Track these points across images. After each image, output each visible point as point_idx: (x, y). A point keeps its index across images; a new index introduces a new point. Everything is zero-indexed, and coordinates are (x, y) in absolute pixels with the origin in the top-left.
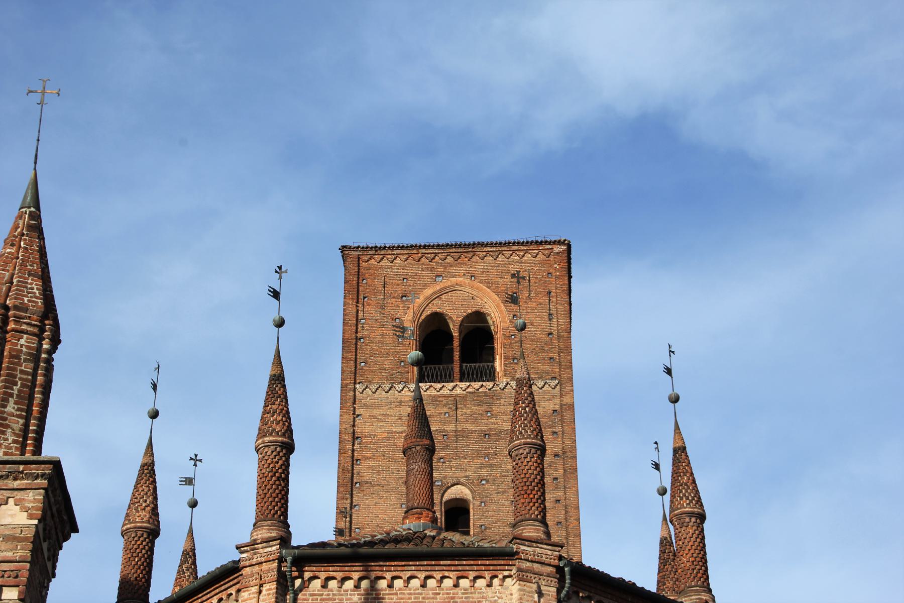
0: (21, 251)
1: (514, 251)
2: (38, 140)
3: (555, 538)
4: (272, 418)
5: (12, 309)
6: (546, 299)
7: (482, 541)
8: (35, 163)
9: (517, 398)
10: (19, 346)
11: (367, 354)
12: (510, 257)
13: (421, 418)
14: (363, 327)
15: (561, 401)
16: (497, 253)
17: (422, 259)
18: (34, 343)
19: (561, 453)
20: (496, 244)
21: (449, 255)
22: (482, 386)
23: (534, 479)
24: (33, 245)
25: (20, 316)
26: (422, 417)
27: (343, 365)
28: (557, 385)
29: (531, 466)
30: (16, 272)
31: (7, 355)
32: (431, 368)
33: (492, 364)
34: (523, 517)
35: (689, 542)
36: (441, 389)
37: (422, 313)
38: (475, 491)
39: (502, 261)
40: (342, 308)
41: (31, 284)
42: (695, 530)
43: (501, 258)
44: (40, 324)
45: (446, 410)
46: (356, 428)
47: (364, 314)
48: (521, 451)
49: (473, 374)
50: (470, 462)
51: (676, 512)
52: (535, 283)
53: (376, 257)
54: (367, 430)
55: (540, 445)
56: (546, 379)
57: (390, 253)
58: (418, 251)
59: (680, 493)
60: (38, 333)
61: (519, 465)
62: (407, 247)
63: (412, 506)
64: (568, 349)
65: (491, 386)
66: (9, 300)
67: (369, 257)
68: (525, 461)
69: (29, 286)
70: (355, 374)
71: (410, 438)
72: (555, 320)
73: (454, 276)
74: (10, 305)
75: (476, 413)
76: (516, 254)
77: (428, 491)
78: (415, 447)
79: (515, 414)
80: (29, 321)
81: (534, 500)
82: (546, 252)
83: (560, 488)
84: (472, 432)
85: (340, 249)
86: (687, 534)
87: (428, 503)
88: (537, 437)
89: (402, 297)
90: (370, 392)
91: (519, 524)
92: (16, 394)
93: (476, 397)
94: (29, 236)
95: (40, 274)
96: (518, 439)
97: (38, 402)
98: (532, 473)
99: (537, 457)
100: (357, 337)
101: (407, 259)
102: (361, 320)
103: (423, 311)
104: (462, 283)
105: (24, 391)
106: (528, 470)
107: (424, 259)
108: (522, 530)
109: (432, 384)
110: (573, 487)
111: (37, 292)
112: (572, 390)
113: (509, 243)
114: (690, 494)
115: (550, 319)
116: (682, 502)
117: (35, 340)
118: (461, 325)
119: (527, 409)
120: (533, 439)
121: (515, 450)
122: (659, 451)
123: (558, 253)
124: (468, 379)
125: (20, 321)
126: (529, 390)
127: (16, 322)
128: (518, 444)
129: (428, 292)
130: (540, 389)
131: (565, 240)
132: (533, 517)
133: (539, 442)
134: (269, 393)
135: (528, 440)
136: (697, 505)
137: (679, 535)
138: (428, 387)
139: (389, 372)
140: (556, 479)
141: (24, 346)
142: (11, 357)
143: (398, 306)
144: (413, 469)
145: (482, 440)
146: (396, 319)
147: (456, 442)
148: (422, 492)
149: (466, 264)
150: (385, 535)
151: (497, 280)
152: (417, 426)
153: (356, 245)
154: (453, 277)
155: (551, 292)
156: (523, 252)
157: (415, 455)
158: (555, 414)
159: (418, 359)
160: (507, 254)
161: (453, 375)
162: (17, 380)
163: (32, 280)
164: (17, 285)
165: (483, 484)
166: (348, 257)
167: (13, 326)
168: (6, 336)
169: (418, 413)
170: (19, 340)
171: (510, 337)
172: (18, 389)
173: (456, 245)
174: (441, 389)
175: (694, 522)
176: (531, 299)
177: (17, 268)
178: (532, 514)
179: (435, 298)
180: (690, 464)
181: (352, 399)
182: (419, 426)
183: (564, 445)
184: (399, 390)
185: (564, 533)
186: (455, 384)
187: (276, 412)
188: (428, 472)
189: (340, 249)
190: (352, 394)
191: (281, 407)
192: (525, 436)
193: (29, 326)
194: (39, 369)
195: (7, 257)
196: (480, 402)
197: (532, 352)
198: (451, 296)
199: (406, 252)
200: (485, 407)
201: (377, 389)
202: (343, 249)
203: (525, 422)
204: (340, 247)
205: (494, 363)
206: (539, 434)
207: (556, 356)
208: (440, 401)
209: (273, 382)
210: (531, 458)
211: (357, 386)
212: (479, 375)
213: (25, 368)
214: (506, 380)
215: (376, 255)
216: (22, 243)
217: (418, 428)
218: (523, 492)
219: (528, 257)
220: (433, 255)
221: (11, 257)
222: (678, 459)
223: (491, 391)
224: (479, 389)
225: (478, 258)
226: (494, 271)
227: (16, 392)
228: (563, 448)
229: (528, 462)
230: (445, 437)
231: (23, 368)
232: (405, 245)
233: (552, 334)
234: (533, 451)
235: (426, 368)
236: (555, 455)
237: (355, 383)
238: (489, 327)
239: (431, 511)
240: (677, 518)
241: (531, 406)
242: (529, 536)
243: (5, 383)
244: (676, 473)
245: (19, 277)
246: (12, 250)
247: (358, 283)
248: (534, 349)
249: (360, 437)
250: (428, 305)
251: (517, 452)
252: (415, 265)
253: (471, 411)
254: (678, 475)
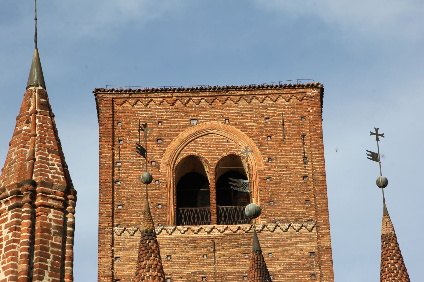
0: (37, 128)
1: (267, 95)
2: (36, 19)
4: (147, 273)
5: (39, 184)
6: (300, 142)
8: (36, 42)
10: (48, 220)
11: (124, 197)
12: (263, 101)
13: (261, 270)
14: (119, 170)
15: (318, 243)
16: (251, 97)
17: (176, 102)
18: (60, 217)
20: (250, 87)
21: (203, 99)
22: (239, 228)
24: (47, 122)
25: (46, 192)
26: (263, 269)
27: (100, 208)
28: (313, 227)
30: (36, 149)
31: (38, 229)
32: (188, 210)
36: (198, 231)
37: (177, 156)
39: (255, 105)
40: (98, 151)
41: (52, 160)
43: (254, 101)
44: (64, 199)
45: (204, 252)
46: (115, 271)
47: (120, 157)
52: (289, 126)
53: (130, 100)
54: (125, 273)
56: (303, 222)
57: (145, 96)
58: (172, 94)
60: (63, 207)
62: (162, 90)
64: (323, 191)
65: (249, 228)
66: (35, 176)
67: (123, 100)
69: (50, 162)
70: (113, 216)
72: (310, 163)
73: (208, 120)
74: (37, 181)
76: (269, 98)
79: (384, 270)
80: (54, 196)
82: (300, 96)
84: (231, 274)
85: (93, 92)
89: (158, 140)
90: (128, 235)
92: (50, 267)
93: (234, 239)
94: (42, 113)
95: (57, 150)
97: (69, 274)
100: (113, 180)
101: (161, 102)
102: (117, 163)
104: (217, 127)
105: (56, 263)
107: (178, 103)
109: (190, 226)
111: (58, 168)
112: (329, 233)
113: (263, 87)
115: (305, 163)
117: (61, 214)
118: (216, 168)
119: (397, 266)
123: (311, 97)
124: (225, 222)
125: (46, 197)
127: (44, 197)
129: (184, 135)
131: (318, 84)
134: (143, 249)
138: (186, 229)
141: (52, 221)
142: (43, 231)
146: (152, 162)
149: (220, 107)
151: (251, 124)
153: (110, 88)
154: (208, 120)
155: (304, 136)
156: (276, 96)
160: (261, 97)
162: (50, 253)
163: (52, 156)
164: (40, 162)
166: (102, 100)
167: (41, 201)
168: (35, 211)
169: (259, 265)
170: (47, 215)
171: (265, 180)
172: (51, 261)
173: (210, 89)
174: (198, 231)
176: (285, 142)
177: (36, 145)
179: (191, 141)
181: (110, 241)
186: (212, 226)
187: (151, 268)
189: (93, 92)
190: (110, 236)
191: (155, 263)
193: (55, 201)
194: (66, 242)
195: (25, 134)
196: (238, 244)
197: (288, 195)
199: (160, 95)
200: (243, 249)
201: (135, 231)
202: (97, 92)
203: (396, 279)
204: (94, 90)
207: (311, 199)
208: (198, 243)
209: (145, 238)
211: (115, 229)
213: (55, 241)
214: (263, 223)
215: (130, 98)
216: (37, 121)
217: (260, 279)
219: (281, 100)
220: (187, 98)
221: (29, 135)
225: (232, 102)
226: (248, 115)
227: (49, 265)
230: (204, 279)
231: (53, 241)
232: (159, 88)
233: (307, 177)
235: (183, 211)
237: (113, 226)
238: (243, 170)
241: (400, 262)
243: (40, 256)
245: (41, 154)
246: (28, 128)
247: (113, 126)
248: (290, 192)
249: (119, 280)
250: (183, 148)
252: (169, 108)
253: (229, 254)
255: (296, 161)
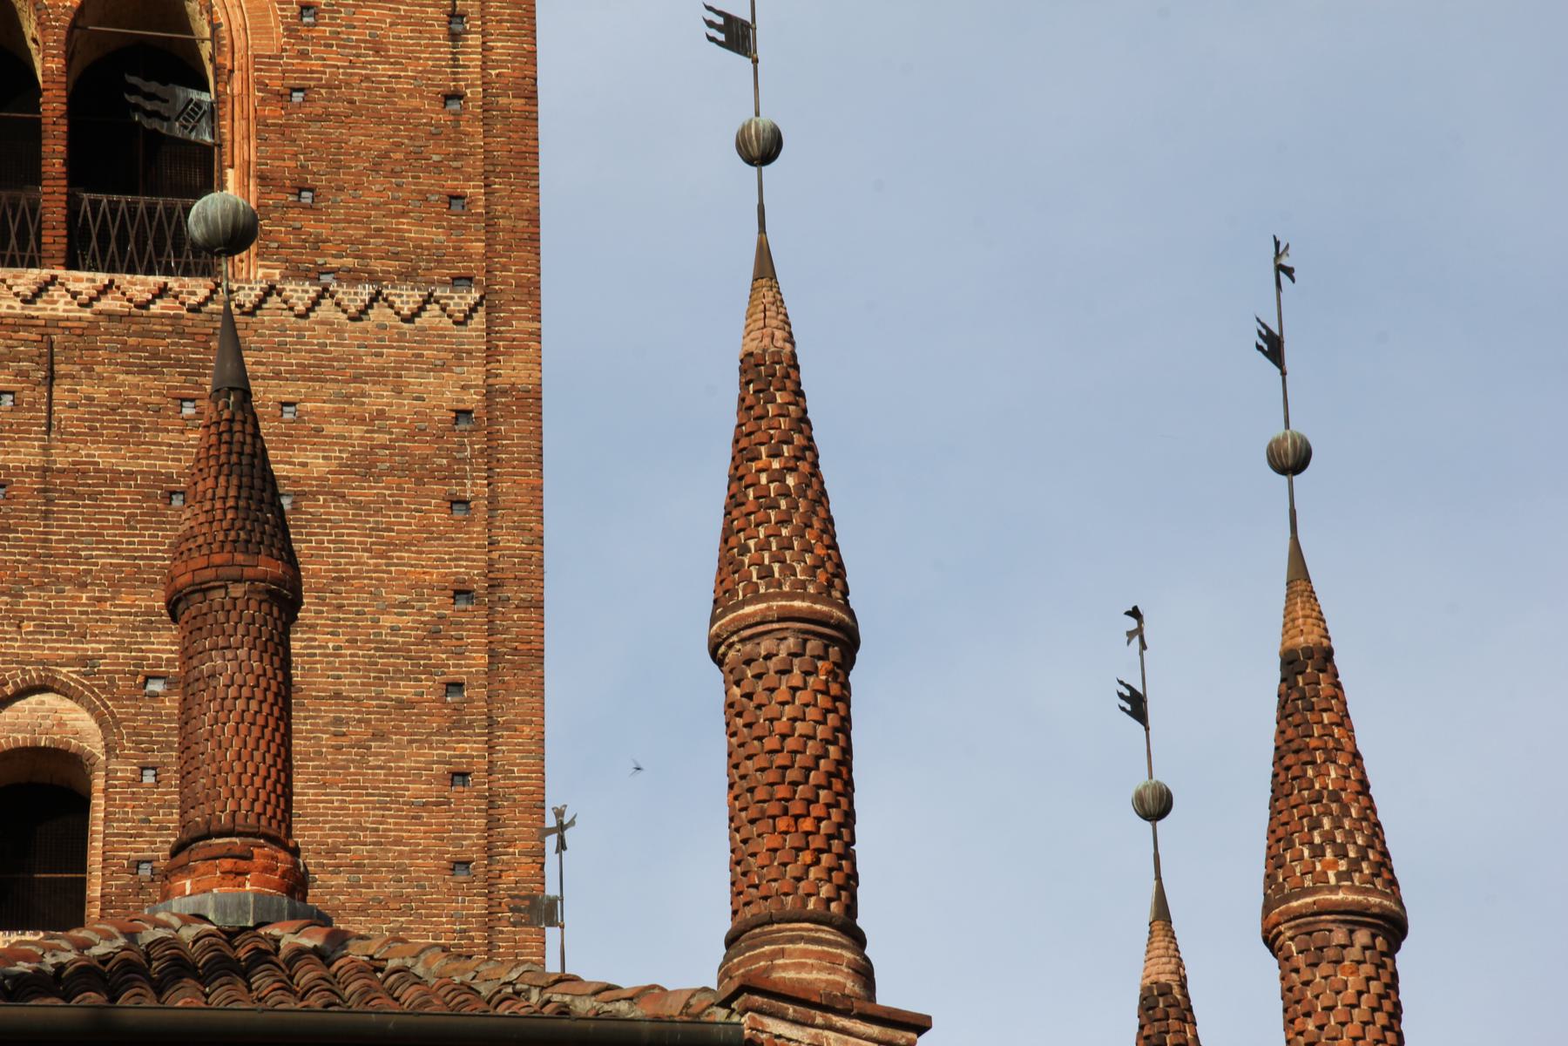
3: (887, 997)
7: (560, 987)
9: (749, 434)
13: (246, 469)
19: (479, 586)
22: (162, 292)
23: (818, 758)
26: (252, 466)
28: (473, 309)
29: (807, 705)
34: (770, 907)
35: (1343, 1024)
38: (118, 723)
42: (1368, 979)
48: (766, 645)
49: (122, 240)
50: (100, 600)
51: (1294, 904)
55: (840, 626)
56: (433, 283)
59: (1311, 829)
61: (757, 700)
63: (208, 823)
65: (203, 293)
68: (783, 687)
71: (205, 550)
72: (474, 40)
75: (133, 403)
77: (275, 765)
78: (226, 587)
79: (740, 498)
81: (817, 842)
83: (470, 726)
84: (115, 478)
86: (1338, 993)
87: (274, 816)
88: (830, 595)
91: (757, 931)
93: (136, 334)
96: (758, 598)
98: (809, 732)
99: (828, 673)
106: (794, 720)
108: (773, 956)
110: (523, 722)
112: (537, 335)
114: (1350, 835)
115: (454, 37)
116: (1319, 867)
118: (73, 26)
119: (791, 481)
120: (814, 599)
121: (742, 641)
122: (1143, 646)
124: (103, 261)
128: (758, 619)
130: (406, 320)
132: (811, 906)
133: (837, 613)
135: (797, 604)
136: (1378, 882)
137: (1303, 993)
140: (455, 686)
144: (212, 676)
145: (155, 512)
147: (46, 515)
148: (251, 770)
150: (121, 941)
152: (231, 503)
157: (221, 617)
158: (462, 426)
165: (154, 696)
169: (236, 448)
171: (283, 96)
175: (1365, 948)
178: (809, 895)
180: (1347, 716)
182: (242, 503)
183: (495, 555)
185: (479, 907)
186: (46, 273)
188: (274, 688)
192: (786, 588)
196: (154, 356)
197: (376, 168)
200: (173, 378)
203: (785, 532)
206: (837, 581)
207: (473, 189)
210: (807, 673)
214: (266, 276)
217: (236, 508)
218: (772, 808)
222: (1303, 698)
223: (202, 316)
224: (150, 302)
228: (491, 564)
229: (794, 689)
234: (813, 645)
236: (457, 592)
239: (285, 848)
240: (1297, 926)
241: (804, 466)
242: (800, 981)
244: (1297, 752)
248: (386, 155)
251: (749, 647)
253: (111, 394)
254: (1305, 757)
255: (420, 25)
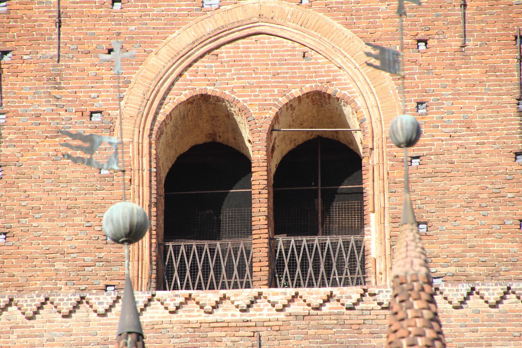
9: (395, 331)
32: (189, 249)
33: (358, 237)
90: (20, 317)
103: (167, 93)
118: (272, 130)
126: (429, 309)
138: (182, 300)
139: (74, 260)
143: (98, 78)
159: (131, 226)
161: (251, 267)
179: (202, 56)
184: (101, 310)
198: (247, 49)
205: (363, 235)
212: (322, 269)
235: (176, 249)
238: (349, 135)
250: (180, 75)
